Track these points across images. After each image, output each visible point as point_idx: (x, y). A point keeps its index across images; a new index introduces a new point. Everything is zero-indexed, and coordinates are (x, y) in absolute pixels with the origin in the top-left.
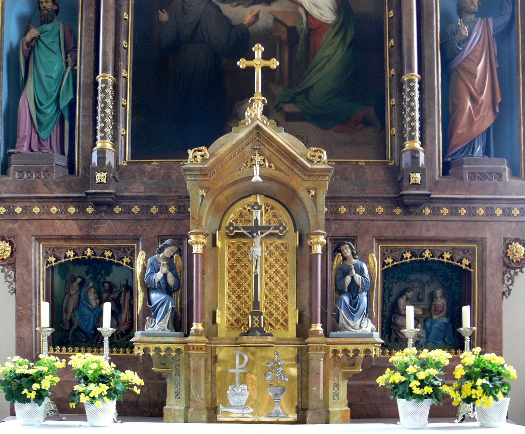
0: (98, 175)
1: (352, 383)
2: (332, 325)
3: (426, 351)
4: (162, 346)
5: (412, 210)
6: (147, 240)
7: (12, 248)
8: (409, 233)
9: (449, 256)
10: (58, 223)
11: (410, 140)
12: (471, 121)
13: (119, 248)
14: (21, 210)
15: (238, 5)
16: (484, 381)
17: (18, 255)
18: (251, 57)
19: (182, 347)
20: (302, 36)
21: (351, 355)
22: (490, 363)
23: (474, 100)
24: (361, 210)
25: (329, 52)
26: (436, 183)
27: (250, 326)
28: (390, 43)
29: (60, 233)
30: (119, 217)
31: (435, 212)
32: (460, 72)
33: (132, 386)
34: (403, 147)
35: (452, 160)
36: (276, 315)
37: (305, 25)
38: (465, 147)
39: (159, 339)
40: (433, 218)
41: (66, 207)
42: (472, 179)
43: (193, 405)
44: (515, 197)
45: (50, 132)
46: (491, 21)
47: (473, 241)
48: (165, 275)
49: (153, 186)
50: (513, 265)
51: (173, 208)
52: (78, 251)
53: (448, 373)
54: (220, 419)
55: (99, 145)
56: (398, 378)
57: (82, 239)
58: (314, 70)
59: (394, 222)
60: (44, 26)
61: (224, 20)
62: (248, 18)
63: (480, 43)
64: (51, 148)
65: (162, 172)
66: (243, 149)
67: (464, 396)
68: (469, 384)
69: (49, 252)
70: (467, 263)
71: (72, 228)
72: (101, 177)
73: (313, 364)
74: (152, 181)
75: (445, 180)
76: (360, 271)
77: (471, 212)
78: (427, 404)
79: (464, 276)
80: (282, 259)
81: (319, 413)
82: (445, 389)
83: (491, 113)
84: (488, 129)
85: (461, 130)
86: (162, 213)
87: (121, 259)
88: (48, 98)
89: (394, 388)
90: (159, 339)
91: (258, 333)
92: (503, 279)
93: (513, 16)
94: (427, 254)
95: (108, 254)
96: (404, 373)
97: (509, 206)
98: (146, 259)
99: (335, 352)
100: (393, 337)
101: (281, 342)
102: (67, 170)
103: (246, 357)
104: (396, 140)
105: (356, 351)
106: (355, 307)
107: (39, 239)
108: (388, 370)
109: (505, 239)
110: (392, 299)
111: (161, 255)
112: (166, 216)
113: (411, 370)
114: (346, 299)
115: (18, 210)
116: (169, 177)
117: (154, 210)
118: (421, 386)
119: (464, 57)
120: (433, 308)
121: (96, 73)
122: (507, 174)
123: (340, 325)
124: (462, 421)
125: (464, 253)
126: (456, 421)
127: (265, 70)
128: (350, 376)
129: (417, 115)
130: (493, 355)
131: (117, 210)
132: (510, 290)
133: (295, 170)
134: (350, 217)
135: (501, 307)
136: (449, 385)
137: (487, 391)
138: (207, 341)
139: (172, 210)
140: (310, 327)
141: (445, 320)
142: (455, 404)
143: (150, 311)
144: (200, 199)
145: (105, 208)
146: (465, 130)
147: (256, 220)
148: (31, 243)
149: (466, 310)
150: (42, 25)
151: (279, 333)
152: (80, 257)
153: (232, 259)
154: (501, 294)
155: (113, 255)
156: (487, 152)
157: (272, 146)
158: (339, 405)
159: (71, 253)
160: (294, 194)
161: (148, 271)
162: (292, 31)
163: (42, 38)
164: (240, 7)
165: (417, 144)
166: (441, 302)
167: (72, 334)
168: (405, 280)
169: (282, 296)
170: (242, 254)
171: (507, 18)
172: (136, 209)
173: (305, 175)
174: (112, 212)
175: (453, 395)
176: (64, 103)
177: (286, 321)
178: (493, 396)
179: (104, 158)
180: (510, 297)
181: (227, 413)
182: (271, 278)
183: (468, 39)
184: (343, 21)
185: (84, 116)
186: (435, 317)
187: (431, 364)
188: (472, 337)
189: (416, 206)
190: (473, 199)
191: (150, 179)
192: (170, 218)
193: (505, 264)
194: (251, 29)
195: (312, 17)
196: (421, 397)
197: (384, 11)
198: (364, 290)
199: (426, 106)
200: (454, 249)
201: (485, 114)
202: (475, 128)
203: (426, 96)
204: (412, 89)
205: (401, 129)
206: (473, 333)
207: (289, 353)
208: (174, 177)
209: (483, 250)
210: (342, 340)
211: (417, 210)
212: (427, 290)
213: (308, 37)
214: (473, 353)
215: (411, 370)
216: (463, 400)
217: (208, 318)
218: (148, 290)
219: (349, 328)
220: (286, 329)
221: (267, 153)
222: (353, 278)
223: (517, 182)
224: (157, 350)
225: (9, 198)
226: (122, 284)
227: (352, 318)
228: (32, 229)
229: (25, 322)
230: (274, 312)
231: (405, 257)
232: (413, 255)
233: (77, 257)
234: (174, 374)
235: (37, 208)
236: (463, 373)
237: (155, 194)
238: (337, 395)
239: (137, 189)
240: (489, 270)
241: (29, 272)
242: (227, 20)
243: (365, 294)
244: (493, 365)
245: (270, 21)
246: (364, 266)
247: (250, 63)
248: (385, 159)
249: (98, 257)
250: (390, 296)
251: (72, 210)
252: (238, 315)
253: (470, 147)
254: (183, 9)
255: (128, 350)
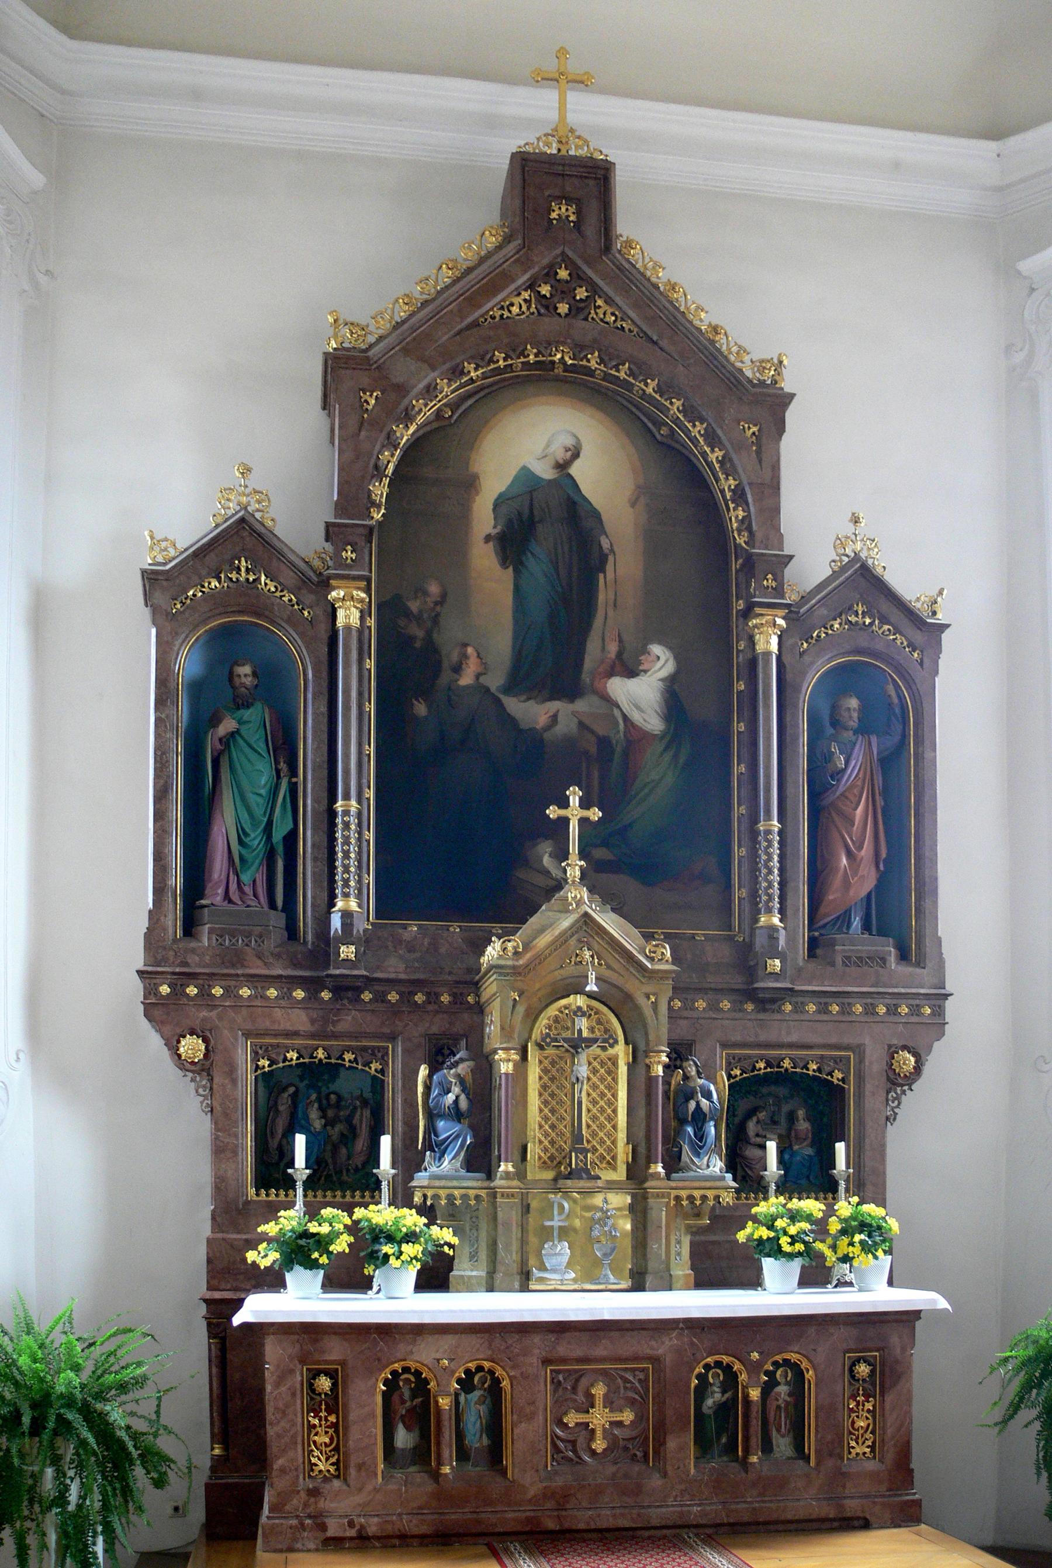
0: (343, 948)
1: (697, 1238)
2: (673, 1164)
3: (795, 1200)
4: (456, 1192)
5: (768, 1006)
6: (409, 1040)
7: (207, 1048)
8: (763, 1037)
9: (815, 1067)
10: (278, 1013)
11: (766, 913)
12: (847, 884)
13: (364, 1049)
14: (221, 991)
15: (529, 699)
16: (862, 1237)
17: (217, 1058)
18: (564, 804)
19: (483, 1193)
20: (619, 750)
21: (698, 1203)
22: (870, 1215)
23: (849, 854)
24: (701, 1004)
25: (654, 776)
26: (800, 970)
27: (573, 1166)
28: (738, 769)
29: (282, 1027)
30: (369, 1007)
31: (798, 1009)
32: (834, 815)
33: (442, 1246)
34: (757, 921)
35: (821, 935)
36: (601, 1150)
37: (622, 734)
38: (838, 918)
39: (455, 1183)
40: (796, 1017)
41: (290, 991)
42: (847, 965)
43: (501, 1268)
44: (903, 991)
45: (253, 874)
46: (874, 739)
47: (847, 1048)
48: (457, 1097)
49: (416, 965)
50: (900, 1081)
51: (446, 995)
52: (304, 1052)
53: (820, 1227)
54: (532, 1287)
55: (340, 904)
56: (764, 1233)
57: (313, 1036)
58: (634, 802)
59: (745, 1025)
60: (242, 711)
61: (509, 721)
62: (542, 720)
63: (860, 776)
64: (255, 895)
65: (426, 941)
66: (566, 941)
67: (840, 1254)
68: (845, 1240)
69: (260, 1052)
70: (840, 1076)
71: (300, 1020)
72: (347, 952)
73: (653, 1214)
74: (413, 956)
75: (811, 966)
76: (708, 1095)
77: (846, 1010)
78: (796, 1265)
79: (837, 1093)
80: (609, 1078)
81: (662, 1277)
82: (819, 1246)
83: (873, 869)
84: (869, 896)
85: (833, 895)
86: (430, 1003)
87: (367, 1064)
88: (255, 825)
89: (758, 1245)
90: (455, 1183)
91: (584, 1176)
92: (887, 1100)
93: (904, 736)
94: (787, 1064)
95: (348, 1056)
96: (771, 1227)
97: (895, 1002)
98: (430, 1076)
99: (678, 1198)
100: (748, 1179)
101: (612, 1186)
102: (286, 934)
103: (566, 1205)
104: (747, 906)
105: (704, 1198)
106: (701, 1141)
107: (247, 1035)
108: (750, 1223)
109: (890, 1046)
110: (737, 1120)
111: (452, 1071)
112: (436, 1007)
113: (780, 1223)
114: (690, 1130)
115: (218, 991)
116: (436, 950)
117: (419, 998)
118: (792, 1244)
119: (838, 793)
120: (793, 1134)
121: (332, 798)
122: (892, 959)
123: (682, 1164)
124: (836, 1286)
125: (836, 1062)
126: (829, 1286)
127: (583, 821)
128: (694, 1230)
129: (775, 877)
130: (872, 1205)
131: (367, 996)
132: (896, 1114)
133: (632, 969)
134: (686, 1014)
135: (884, 1137)
136: (823, 1241)
137: (866, 1248)
138: (522, 1186)
139: (445, 998)
140: (649, 1167)
141: (810, 1151)
142: (828, 1264)
143: (436, 1147)
144: (511, 1003)
145: (350, 994)
146: (838, 895)
147: (580, 1031)
148: (237, 1040)
149: (840, 1147)
150: (238, 708)
151: (608, 1175)
152: (307, 1060)
153: (546, 1078)
154: (884, 1119)
155: (355, 1059)
156: (867, 927)
157: (603, 938)
158: (682, 1269)
159: (293, 1055)
160: (628, 997)
161: (435, 1092)
162: (604, 743)
163: (243, 732)
164: (531, 702)
165: (776, 920)
166: (803, 1125)
167: (343, 1175)
168: (755, 1094)
169: (609, 1126)
170: (558, 1071)
171: (897, 738)
172: (393, 997)
173: (644, 977)
174: (358, 1000)
175: (828, 1253)
176: (279, 834)
177: (614, 1158)
178: (873, 1254)
179: (352, 925)
180: (895, 1123)
181: (541, 1280)
182: (594, 1102)
183: (844, 770)
184: (675, 729)
185: (315, 859)
186: (796, 1147)
187: (801, 1216)
188: (847, 1181)
189: (773, 1001)
190: (848, 993)
191: (409, 952)
192: (441, 1009)
193: (889, 1079)
194: (547, 736)
195: (632, 723)
196: (790, 1256)
197: (730, 721)
198: (712, 1119)
199: (789, 864)
200: (822, 1057)
201: (865, 873)
202: (852, 893)
203: (789, 850)
204: (770, 843)
205: (754, 895)
206: (849, 1176)
207: (620, 1200)
208: (443, 950)
209: (861, 1060)
210: (687, 1184)
211: (775, 1006)
212: (785, 1109)
213: (626, 754)
214: (849, 1203)
215: (780, 1223)
216: (838, 1259)
217: (517, 1156)
218: (431, 1117)
219: (694, 1168)
220: (615, 1169)
221: (596, 947)
222: (698, 1103)
223: (905, 970)
224: (450, 1198)
225: (204, 974)
226: (354, 1095)
227: (698, 1155)
228: (239, 1019)
229: (229, 1154)
230: (598, 1147)
231: (758, 1066)
232: (769, 1064)
233: (302, 1060)
234: (468, 1229)
235: (245, 989)
236: (839, 1227)
237: (422, 976)
238: (679, 1254)
239: (394, 967)
240: (869, 1087)
241: (234, 1082)
242: (512, 721)
243: (712, 1123)
244: (873, 1218)
245: (574, 726)
246: (712, 1087)
247: (562, 812)
248: (730, 930)
249: (333, 1061)
250: (734, 1115)
251: (299, 994)
252: (553, 1151)
253: (844, 920)
254: (449, 700)
255: (367, 1193)
